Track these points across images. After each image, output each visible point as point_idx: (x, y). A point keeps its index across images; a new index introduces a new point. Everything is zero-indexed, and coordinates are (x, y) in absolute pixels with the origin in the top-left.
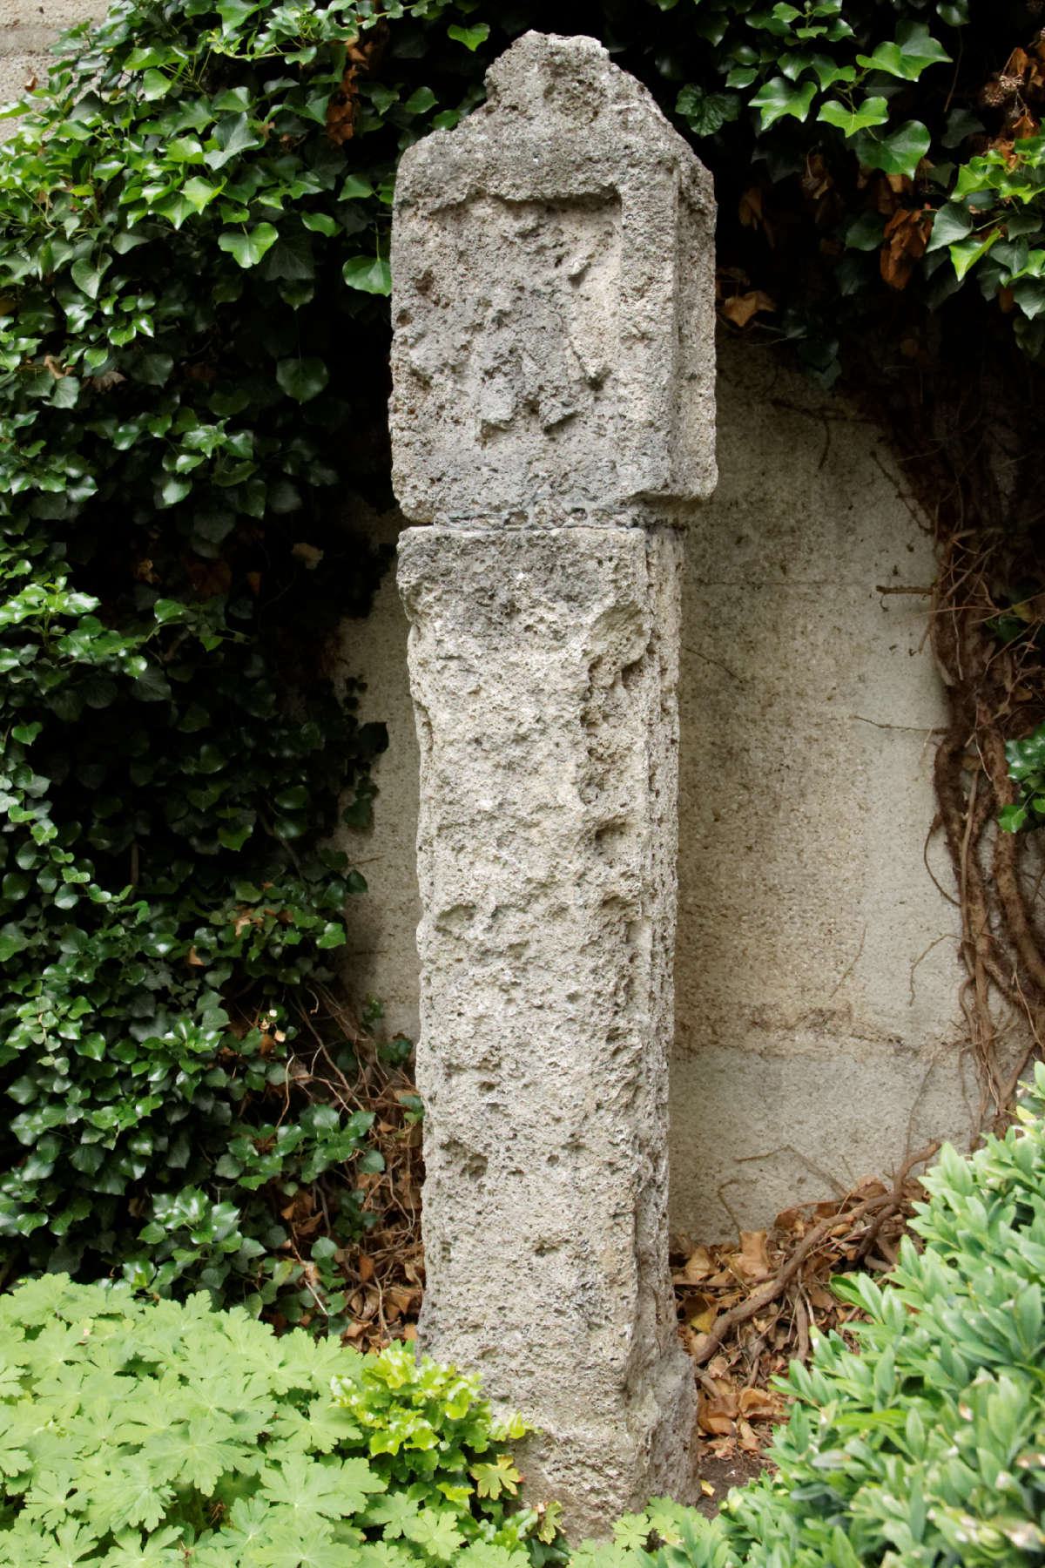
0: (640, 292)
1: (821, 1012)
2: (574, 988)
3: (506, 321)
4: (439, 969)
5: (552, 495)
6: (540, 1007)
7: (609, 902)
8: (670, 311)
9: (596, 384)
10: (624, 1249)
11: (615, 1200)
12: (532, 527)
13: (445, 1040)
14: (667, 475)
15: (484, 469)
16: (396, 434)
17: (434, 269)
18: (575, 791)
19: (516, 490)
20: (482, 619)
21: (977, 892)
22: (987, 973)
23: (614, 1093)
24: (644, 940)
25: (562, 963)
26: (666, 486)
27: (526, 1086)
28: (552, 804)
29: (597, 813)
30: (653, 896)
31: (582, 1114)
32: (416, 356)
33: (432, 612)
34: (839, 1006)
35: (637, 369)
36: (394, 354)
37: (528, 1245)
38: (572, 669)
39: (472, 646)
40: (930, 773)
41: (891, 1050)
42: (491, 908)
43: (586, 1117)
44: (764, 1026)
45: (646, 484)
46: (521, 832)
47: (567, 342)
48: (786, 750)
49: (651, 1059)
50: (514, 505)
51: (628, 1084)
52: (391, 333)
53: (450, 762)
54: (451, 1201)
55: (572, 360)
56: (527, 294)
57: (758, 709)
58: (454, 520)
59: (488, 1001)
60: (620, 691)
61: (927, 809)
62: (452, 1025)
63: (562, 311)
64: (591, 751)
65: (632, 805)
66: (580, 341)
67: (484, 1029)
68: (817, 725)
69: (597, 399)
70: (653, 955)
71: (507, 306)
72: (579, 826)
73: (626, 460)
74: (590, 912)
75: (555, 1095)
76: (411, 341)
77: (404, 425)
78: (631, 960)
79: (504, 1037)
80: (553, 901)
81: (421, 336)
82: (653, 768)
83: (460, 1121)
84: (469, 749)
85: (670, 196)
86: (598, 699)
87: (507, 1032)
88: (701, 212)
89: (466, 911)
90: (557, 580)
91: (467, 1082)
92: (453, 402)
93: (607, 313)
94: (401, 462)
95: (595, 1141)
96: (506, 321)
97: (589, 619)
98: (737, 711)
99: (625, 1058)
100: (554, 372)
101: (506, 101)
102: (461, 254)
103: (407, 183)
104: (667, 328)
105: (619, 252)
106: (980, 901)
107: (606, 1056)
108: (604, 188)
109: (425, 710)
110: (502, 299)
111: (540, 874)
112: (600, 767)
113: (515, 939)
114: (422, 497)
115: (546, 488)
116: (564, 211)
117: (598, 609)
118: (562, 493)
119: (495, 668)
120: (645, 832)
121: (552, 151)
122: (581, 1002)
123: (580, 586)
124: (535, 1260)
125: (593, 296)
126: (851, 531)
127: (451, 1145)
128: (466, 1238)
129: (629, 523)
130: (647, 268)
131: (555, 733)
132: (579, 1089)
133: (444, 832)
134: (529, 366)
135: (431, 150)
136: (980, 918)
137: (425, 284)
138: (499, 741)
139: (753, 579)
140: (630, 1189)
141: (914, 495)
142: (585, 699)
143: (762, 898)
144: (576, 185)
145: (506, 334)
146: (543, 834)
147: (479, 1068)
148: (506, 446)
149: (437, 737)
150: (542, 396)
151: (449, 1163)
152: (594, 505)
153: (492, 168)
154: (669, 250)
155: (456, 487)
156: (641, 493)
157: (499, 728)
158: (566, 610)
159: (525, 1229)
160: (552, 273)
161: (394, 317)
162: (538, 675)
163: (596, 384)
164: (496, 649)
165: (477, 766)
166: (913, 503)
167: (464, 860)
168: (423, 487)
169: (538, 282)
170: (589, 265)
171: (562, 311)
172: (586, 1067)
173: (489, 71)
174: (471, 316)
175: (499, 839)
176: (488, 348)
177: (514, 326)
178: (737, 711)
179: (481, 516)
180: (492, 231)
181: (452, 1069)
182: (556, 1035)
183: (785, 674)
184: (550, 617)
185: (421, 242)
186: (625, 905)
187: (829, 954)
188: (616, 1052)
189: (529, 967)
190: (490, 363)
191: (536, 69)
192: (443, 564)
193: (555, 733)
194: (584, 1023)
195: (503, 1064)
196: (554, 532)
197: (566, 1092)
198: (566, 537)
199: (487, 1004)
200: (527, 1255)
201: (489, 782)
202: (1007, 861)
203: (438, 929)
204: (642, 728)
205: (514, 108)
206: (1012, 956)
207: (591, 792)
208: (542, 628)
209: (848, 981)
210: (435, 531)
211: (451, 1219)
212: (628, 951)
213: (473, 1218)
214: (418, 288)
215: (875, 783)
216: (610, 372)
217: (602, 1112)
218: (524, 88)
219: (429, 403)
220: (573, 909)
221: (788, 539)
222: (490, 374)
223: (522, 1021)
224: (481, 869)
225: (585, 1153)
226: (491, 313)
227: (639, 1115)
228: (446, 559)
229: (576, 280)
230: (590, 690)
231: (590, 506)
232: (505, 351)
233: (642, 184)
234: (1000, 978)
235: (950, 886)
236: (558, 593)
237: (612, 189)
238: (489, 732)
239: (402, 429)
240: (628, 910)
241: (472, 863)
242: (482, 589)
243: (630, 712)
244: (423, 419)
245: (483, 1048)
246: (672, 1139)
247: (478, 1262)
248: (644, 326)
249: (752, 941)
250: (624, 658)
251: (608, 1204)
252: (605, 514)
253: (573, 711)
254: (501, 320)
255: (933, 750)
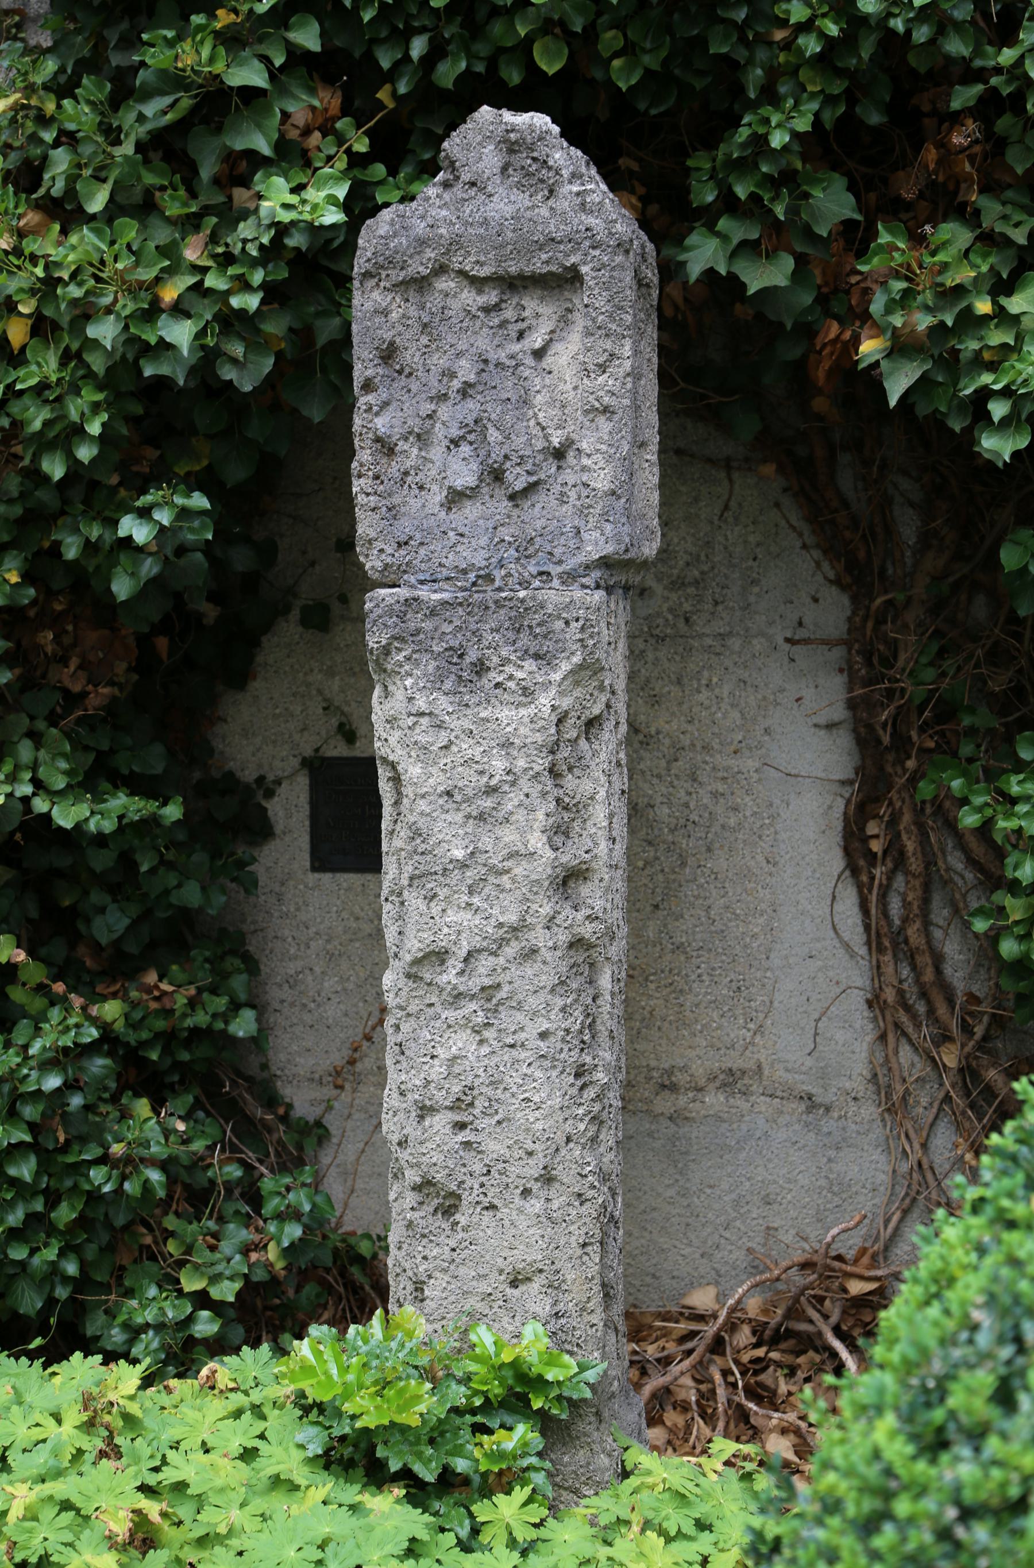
0: (603, 368)
1: (730, 1072)
2: (545, 1026)
3: (470, 392)
4: (409, 1015)
5: (518, 559)
6: (512, 1046)
7: (577, 943)
8: (629, 386)
9: (559, 454)
10: (593, 1278)
11: (584, 1230)
12: (500, 589)
13: (418, 1083)
14: (627, 540)
15: (451, 534)
16: (361, 499)
17: (398, 340)
18: (545, 839)
19: (484, 554)
20: (453, 677)
21: (887, 944)
22: (897, 1025)
23: (582, 1127)
24: (605, 981)
25: (533, 1002)
26: (627, 550)
27: (499, 1122)
28: (523, 852)
29: (564, 859)
30: (613, 938)
31: (554, 1146)
32: (381, 424)
33: (402, 671)
34: (751, 1065)
35: (600, 441)
36: (358, 422)
37: (502, 1278)
38: (541, 723)
39: (444, 703)
40: (839, 825)
41: (802, 1107)
42: (463, 953)
43: (557, 1150)
44: (673, 1088)
45: (609, 549)
46: (492, 879)
47: (531, 413)
48: (692, 805)
49: (611, 1095)
50: (480, 568)
51: (594, 1118)
52: (355, 400)
53: (422, 814)
54: (425, 1241)
55: (536, 431)
56: (491, 367)
57: (663, 763)
58: (422, 582)
59: (461, 1042)
60: (583, 743)
61: (837, 862)
62: (426, 1067)
63: (526, 384)
64: (558, 800)
65: (595, 851)
66: (545, 413)
67: (457, 1069)
68: (724, 779)
69: (559, 468)
70: (613, 994)
71: (472, 378)
72: (549, 871)
73: (590, 526)
74: (559, 953)
75: (528, 1130)
76: (375, 409)
77: (370, 490)
78: (594, 1000)
79: (476, 1076)
80: (523, 944)
81: (386, 404)
82: (611, 815)
83: (434, 1160)
84: (441, 801)
85: (628, 278)
86: (565, 752)
87: (481, 1072)
88: (648, 286)
89: (438, 956)
90: (524, 640)
91: (441, 1122)
92: (418, 469)
93: (569, 387)
94: (366, 526)
95: (566, 1174)
96: (470, 392)
97: (557, 676)
98: (642, 766)
99: (591, 1093)
100: (519, 441)
101: (466, 177)
102: (425, 326)
103: (369, 254)
104: (626, 402)
105: (581, 329)
106: (889, 952)
107: (574, 1091)
108: (566, 268)
109: (393, 766)
110: (466, 371)
111: (512, 918)
112: (566, 816)
113: (487, 982)
114: (389, 560)
115: (512, 551)
116: (525, 288)
117: (565, 667)
118: (527, 557)
119: (467, 724)
120: (606, 877)
121: (514, 231)
122: (552, 1039)
123: (548, 645)
124: (509, 1291)
125: (555, 369)
126: (754, 582)
127: (425, 1186)
128: (438, 1275)
129: (593, 585)
130: (608, 345)
131: (524, 784)
132: (552, 1122)
133: (416, 882)
134: (493, 435)
135: (392, 223)
136: (889, 970)
137: (388, 354)
138: (470, 792)
139: (657, 632)
140: (597, 1218)
141: (818, 546)
142: (552, 752)
143: (669, 957)
144: (538, 265)
145: (470, 404)
146: (513, 880)
147: (451, 1108)
148: (471, 511)
149: (408, 791)
150: (508, 464)
151: (421, 1203)
152: (559, 569)
153: (455, 244)
154: (628, 328)
155: (422, 551)
156: (604, 557)
157: (470, 780)
158: (534, 668)
159: (500, 1260)
160: (516, 347)
161: (357, 385)
162: (508, 729)
163: (559, 454)
164: (467, 705)
165: (449, 817)
166: (817, 554)
167: (436, 909)
168: (389, 551)
169: (502, 355)
170: (551, 340)
171: (526, 384)
172: (557, 1101)
173: (446, 145)
174: (435, 386)
175: (470, 887)
176: (453, 418)
177: (479, 397)
178: (642, 766)
179: (448, 579)
180: (455, 305)
181: (425, 1111)
182: (529, 1072)
183: (690, 728)
184: (520, 675)
185: (385, 313)
186: (590, 946)
187: (739, 1011)
188: (582, 1088)
189: (501, 1008)
190: (455, 432)
191: (492, 147)
192: (412, 625)
193: (524, 784)
194: (554, 1059)
195: (477, 1103)
196: (522, 594)
197: (539, 1126)
198: (533, 598)
199: (460, 1045)
200: (501, 1288)
201: (461, 832)
202: (916, 910)
203: (408, 976)
204: (603, 779)
205: (473, 184)
206: (921, 1008)
207: (558, 840)
208: (511, 684)
209: (758, 1039)
210: (403, 592)
211: (425, 1258)
212: (591, 991)
213: (447, 1254)
214: (382, 358)
215: (783, 836)
216: (573, 442)
217: (571, 1145)
218: (481, 165)
219: (394, 469)
220: (543, 949)
221: (691, 590)
222: (455, 442)
223: (495, 1059)
224: (452, 917)
225: (557, 1185)
226: (456, 384)
227: (602, 1149)
228: (415, 620)
229: (539, 354)
230: (557, 743)
231: (555, 570)
232: (470, 420)
233: (604, 266)
234: (910, 1030)
235: (856, 936)
236: (526, 652)
237: (574, 269)
238: (460, 784)
239: (368, 494)
240: (592, 951)
241: (444, 911)
242: (451, 648)
243: (593, 764)
244: (388, 485)
245: (456, 1089)
246: (623, 1176)
247: (453, 1298)
248: (606, 400)
249: (661, 1002)
250: (588, 713)
251: (578, 1235)
252: (569, 578)
253: (541, 764)
254: (465, 391)
255: (840, 805)
